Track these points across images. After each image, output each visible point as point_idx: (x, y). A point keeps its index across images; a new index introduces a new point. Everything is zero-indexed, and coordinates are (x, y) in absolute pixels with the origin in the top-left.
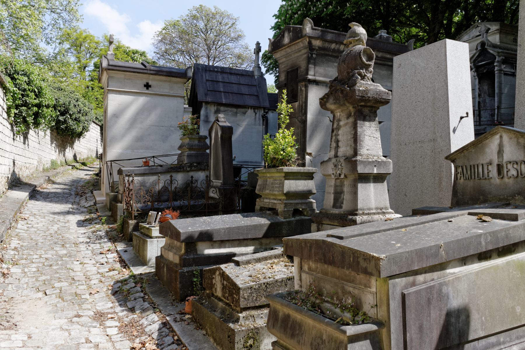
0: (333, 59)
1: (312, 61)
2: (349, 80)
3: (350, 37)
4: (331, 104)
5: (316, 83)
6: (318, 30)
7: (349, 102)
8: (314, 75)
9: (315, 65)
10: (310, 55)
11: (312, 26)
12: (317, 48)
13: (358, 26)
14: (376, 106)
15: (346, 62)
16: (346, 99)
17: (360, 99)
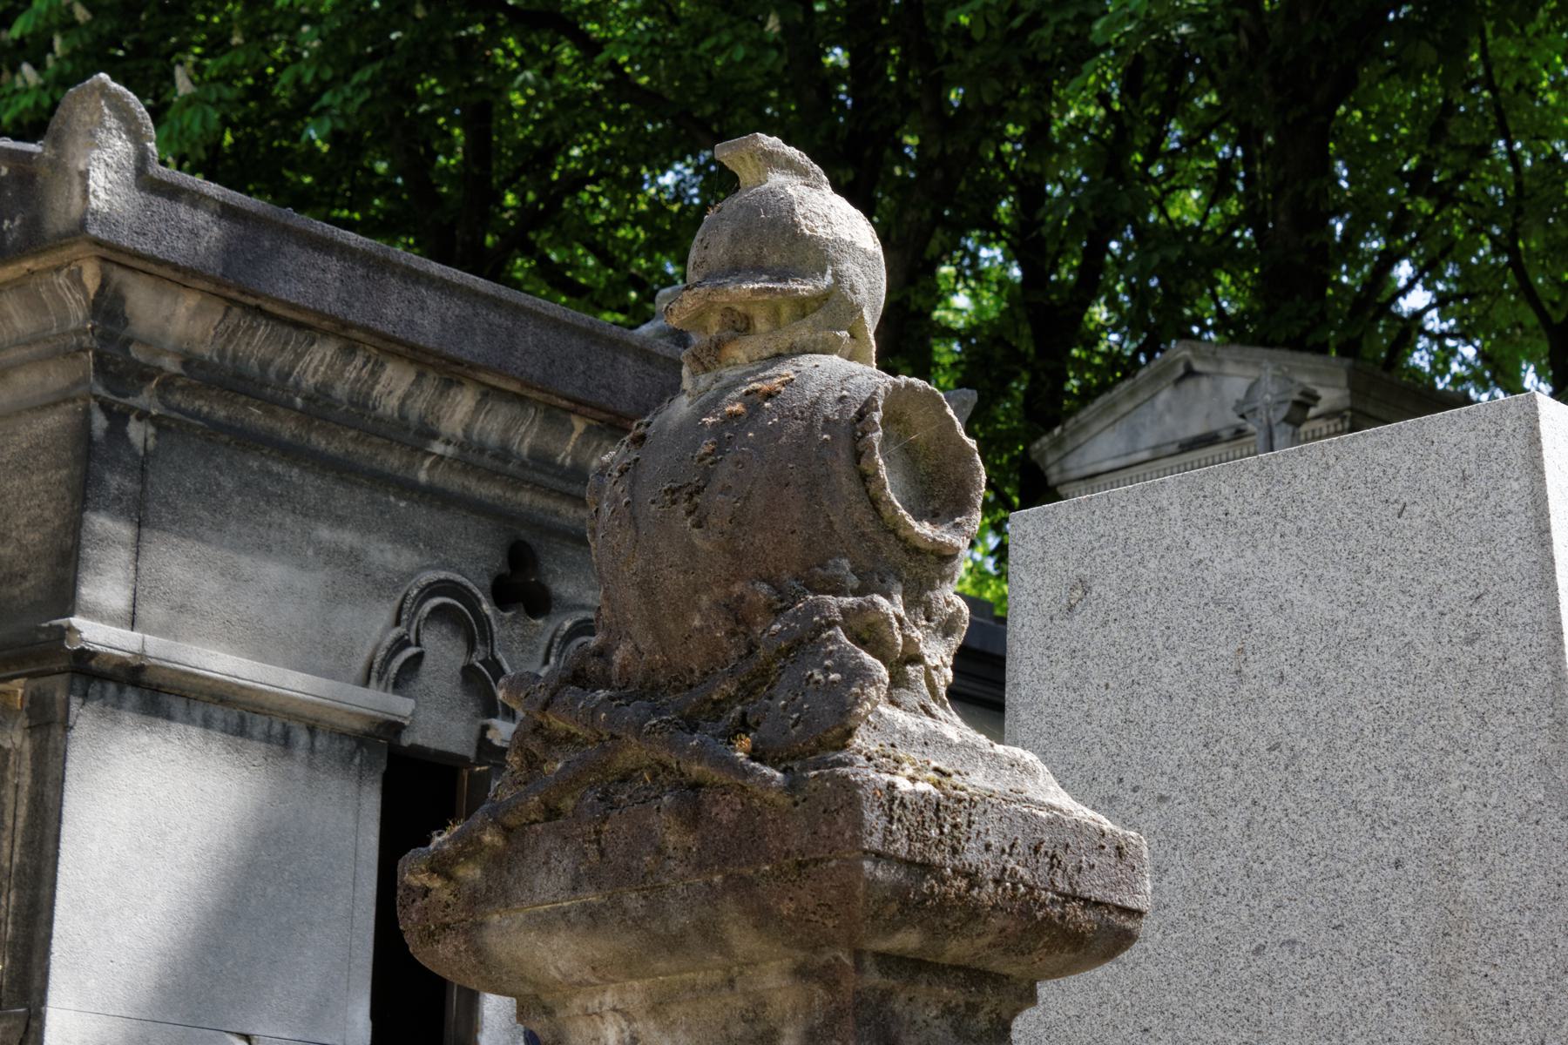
0: (311, 485)
1: (115, 481)
2: (756, 683)
3: (736, 270)
4: (545, 924)
5: (148, 691)
6: (196, 200)
7: (763, 918)
8: (133, 622)
9: (141, 516)
10: (100, 422)
11: (142, 159)
12: (170, 364)
13: (802, 172)
14: (1012, 968)
15: (718, 503)
16: (741, 886)
17: (899, 891)
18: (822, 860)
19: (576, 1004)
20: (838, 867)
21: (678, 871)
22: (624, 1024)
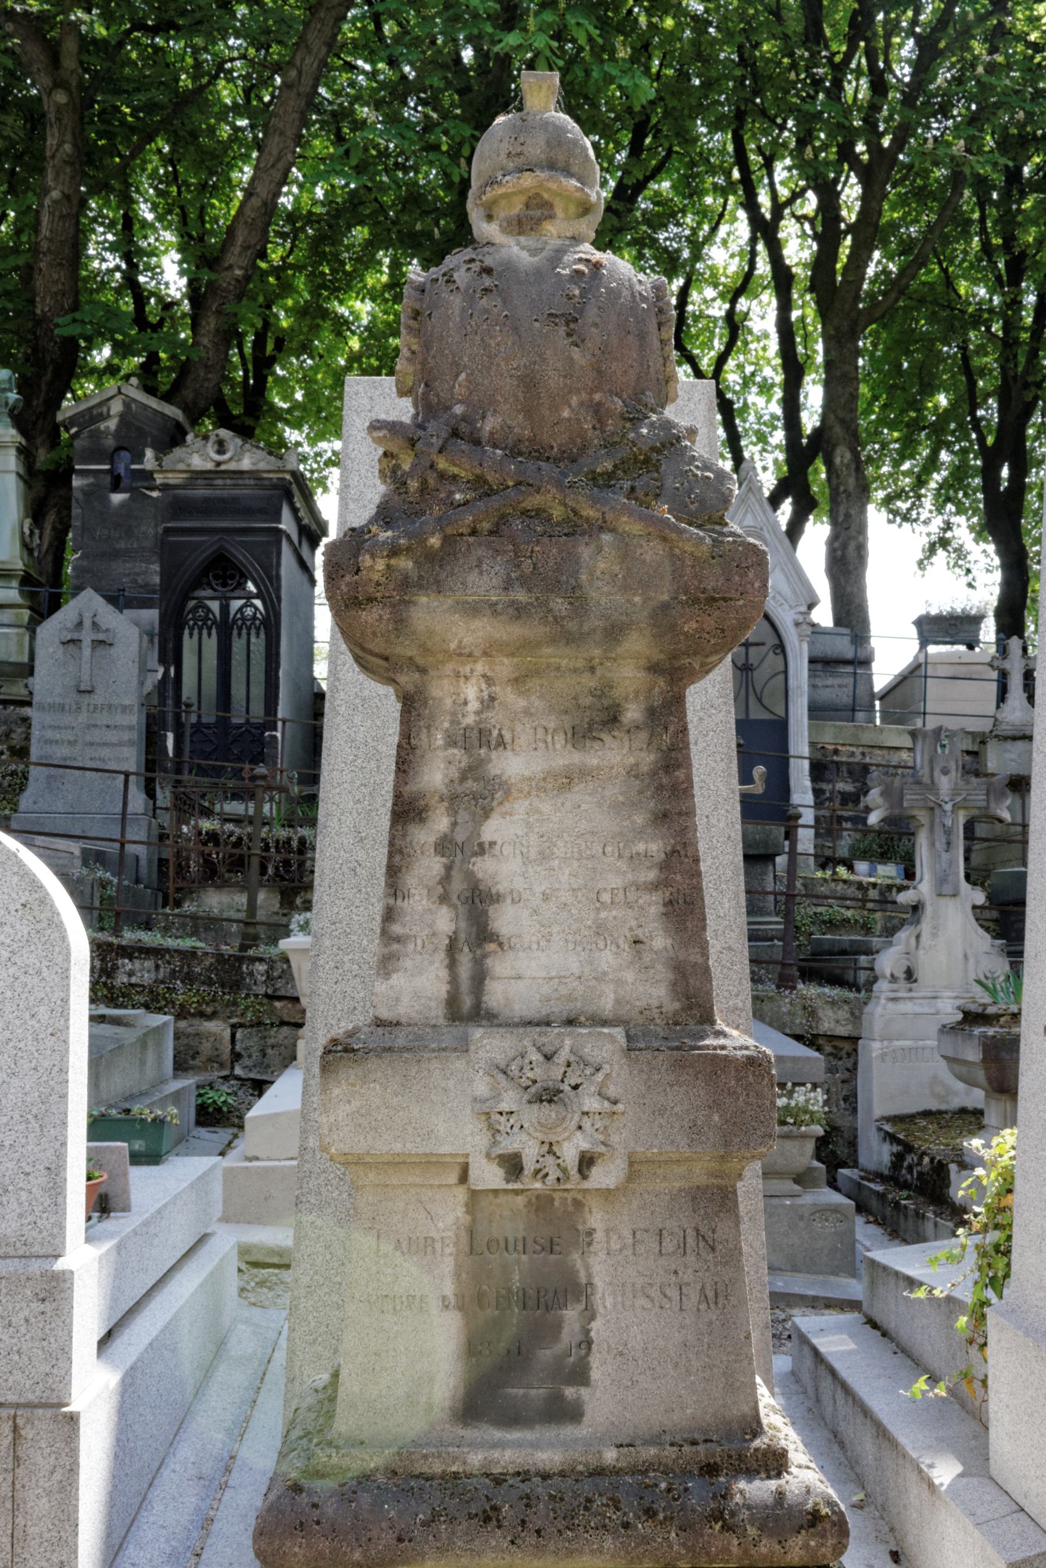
18: (731, 599)
19: (449, 668)
20: (745, 606)
21: (605, 589)
22: (484, 686)
